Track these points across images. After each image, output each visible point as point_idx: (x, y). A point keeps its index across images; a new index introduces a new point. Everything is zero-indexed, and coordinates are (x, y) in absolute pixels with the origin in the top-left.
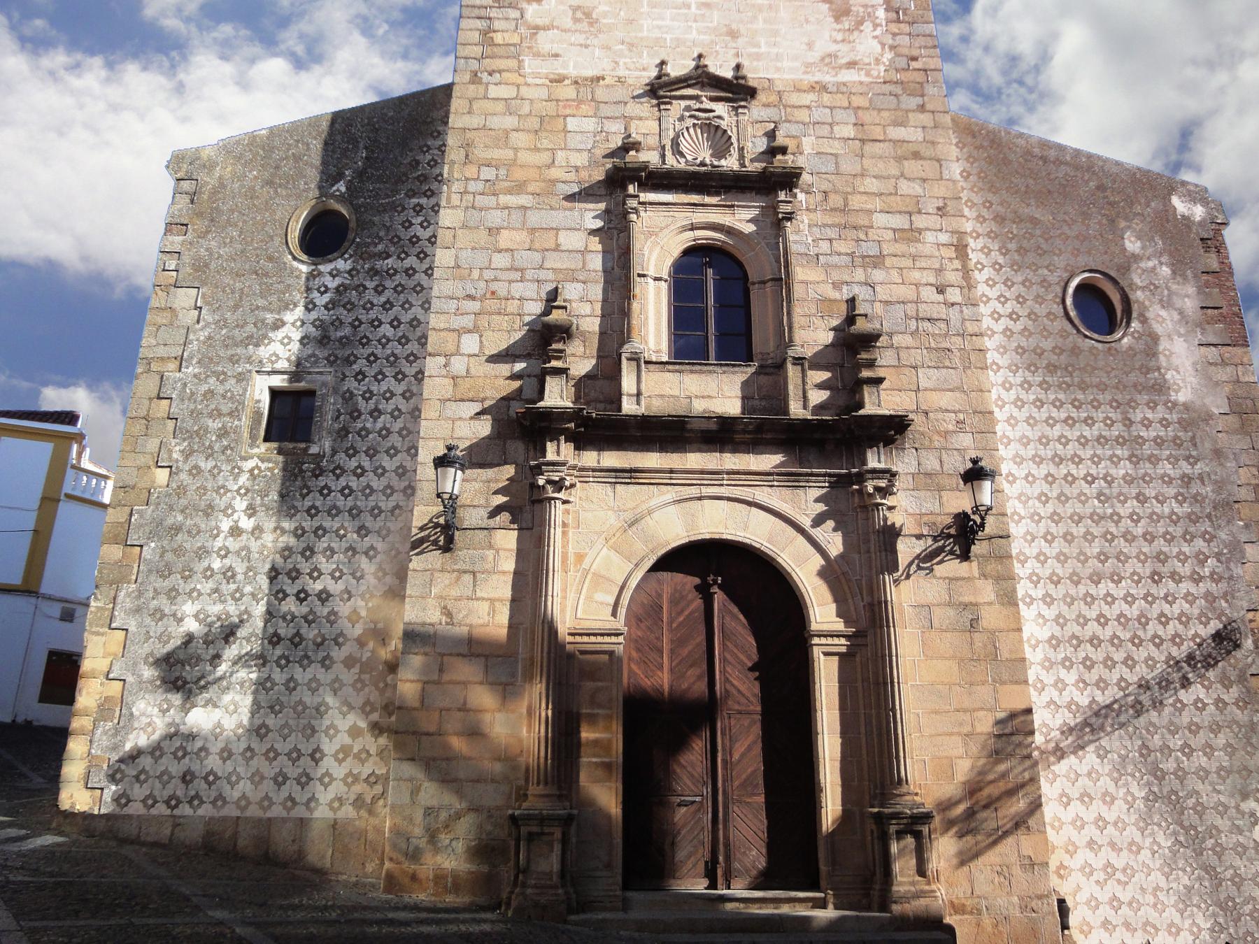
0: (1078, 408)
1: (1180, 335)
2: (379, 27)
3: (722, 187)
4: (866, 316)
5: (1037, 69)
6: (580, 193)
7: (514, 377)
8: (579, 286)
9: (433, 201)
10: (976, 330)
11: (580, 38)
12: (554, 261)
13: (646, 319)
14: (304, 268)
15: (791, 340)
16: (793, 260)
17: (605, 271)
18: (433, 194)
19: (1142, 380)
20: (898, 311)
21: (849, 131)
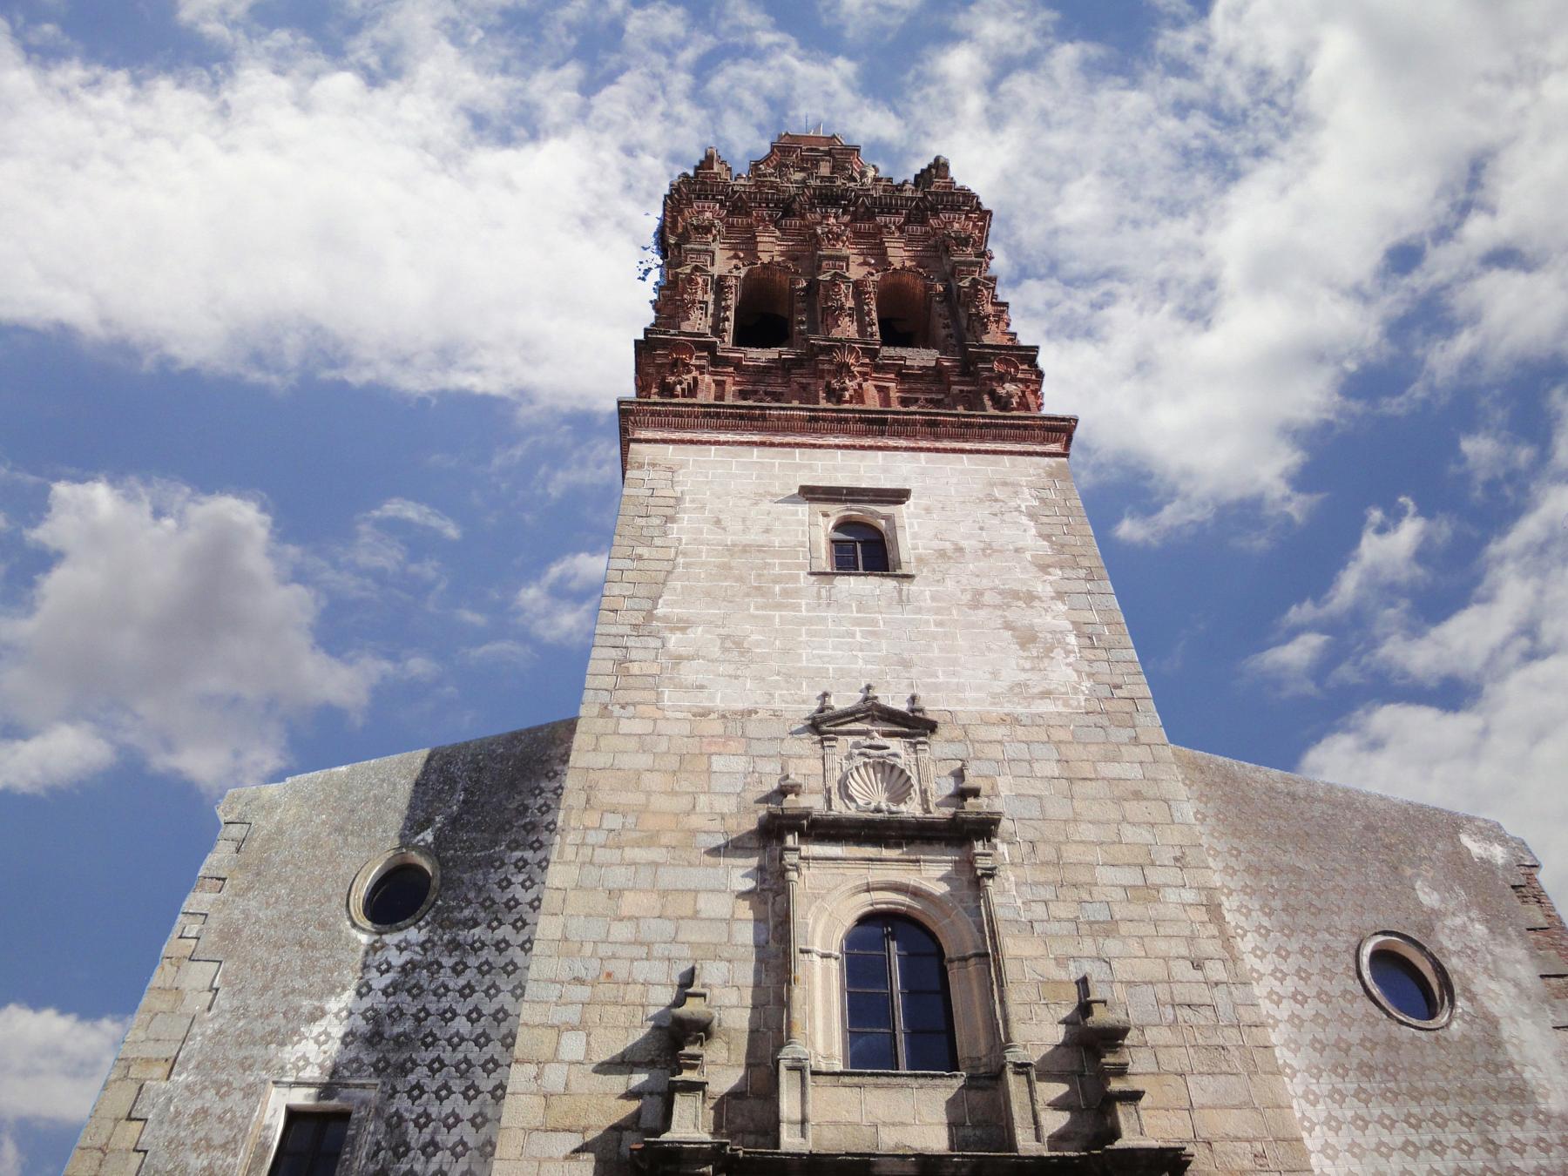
0: (1417, 1127)
1: (1525, 1016)
2: (472, 33)
3: (904, 837)
4: (1105, 1002)
5: (1291, 86)
6: (726, 846)
7: (631, 1095)
8: (723, 965)
9: (540, 854)
10: (1254, 1018)
11: (730, 669)
12: (692, 933)
13: (812, 1010)
14: (364, 939)
15: (1008, 1039)
16: (1001, 928)
17: (757, 946)
18: (542, 845)
19: (1492, 1081)
20: (1146, 994)
21: (1053, 769)
